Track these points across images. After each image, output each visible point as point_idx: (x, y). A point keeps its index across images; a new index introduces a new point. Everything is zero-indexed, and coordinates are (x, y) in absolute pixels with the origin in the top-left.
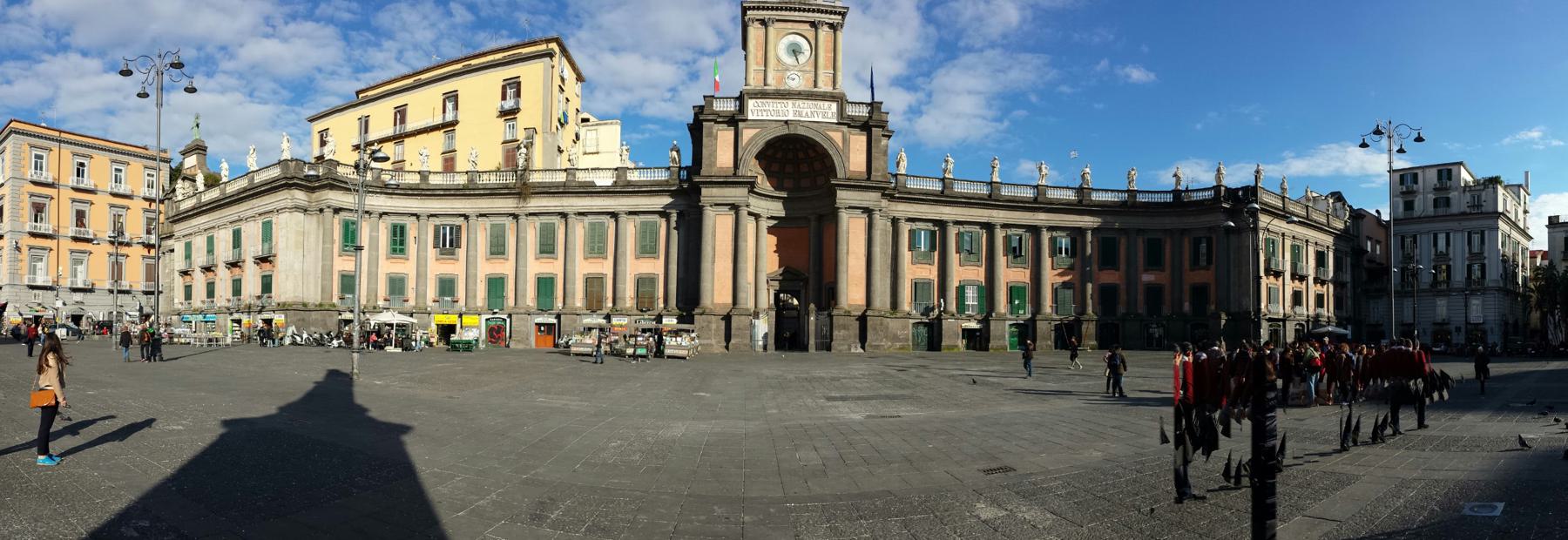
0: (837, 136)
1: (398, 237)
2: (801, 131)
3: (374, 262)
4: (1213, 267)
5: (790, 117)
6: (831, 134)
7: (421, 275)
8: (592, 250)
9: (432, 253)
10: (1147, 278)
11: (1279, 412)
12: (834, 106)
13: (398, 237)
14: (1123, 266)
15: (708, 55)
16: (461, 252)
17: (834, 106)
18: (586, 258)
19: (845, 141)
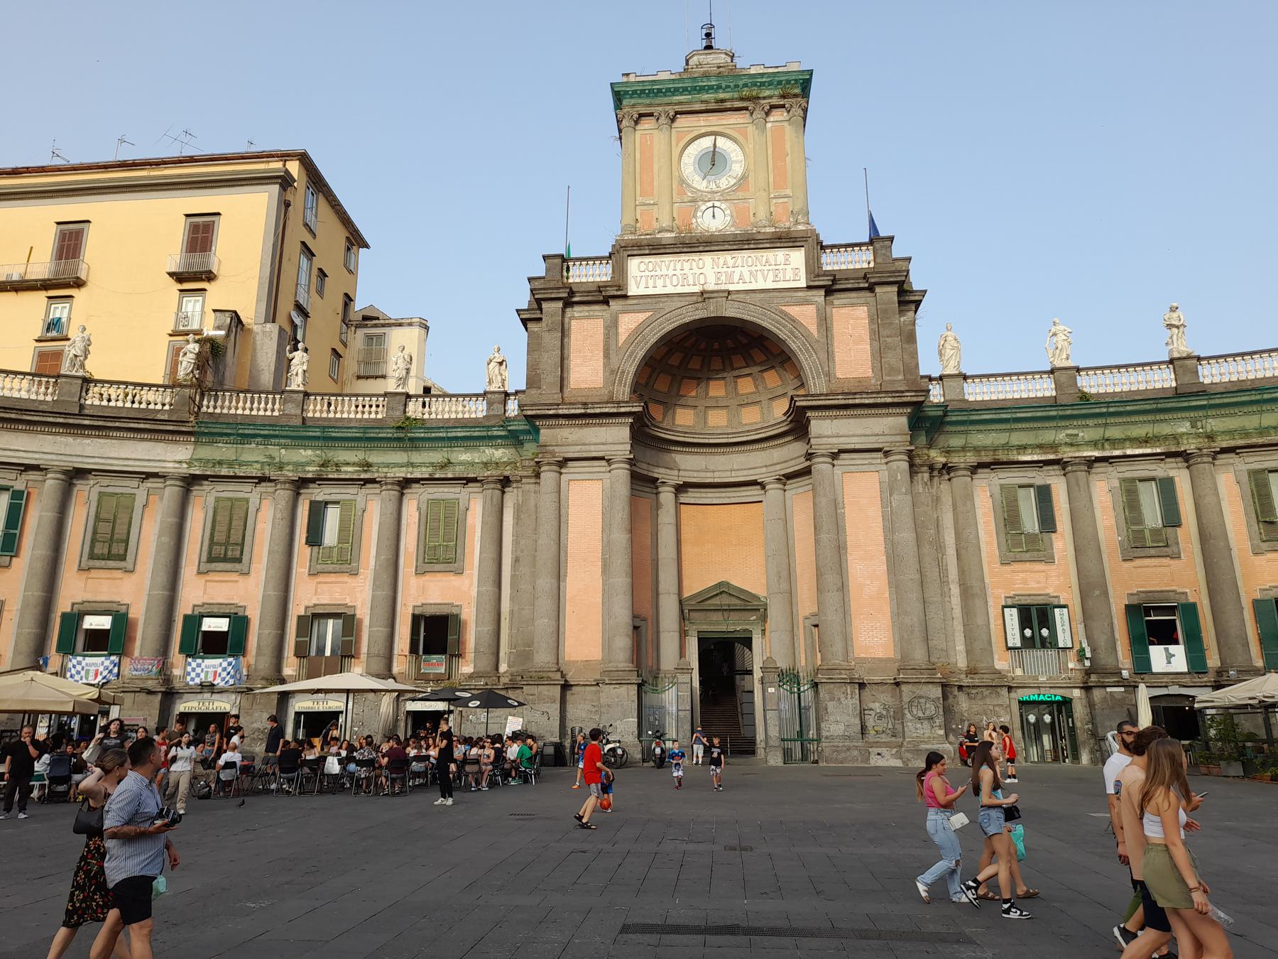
0: (806, 314)
6: (793, 311)
12: (797, 257)
16: (1062, 542)
19: (825, 322)
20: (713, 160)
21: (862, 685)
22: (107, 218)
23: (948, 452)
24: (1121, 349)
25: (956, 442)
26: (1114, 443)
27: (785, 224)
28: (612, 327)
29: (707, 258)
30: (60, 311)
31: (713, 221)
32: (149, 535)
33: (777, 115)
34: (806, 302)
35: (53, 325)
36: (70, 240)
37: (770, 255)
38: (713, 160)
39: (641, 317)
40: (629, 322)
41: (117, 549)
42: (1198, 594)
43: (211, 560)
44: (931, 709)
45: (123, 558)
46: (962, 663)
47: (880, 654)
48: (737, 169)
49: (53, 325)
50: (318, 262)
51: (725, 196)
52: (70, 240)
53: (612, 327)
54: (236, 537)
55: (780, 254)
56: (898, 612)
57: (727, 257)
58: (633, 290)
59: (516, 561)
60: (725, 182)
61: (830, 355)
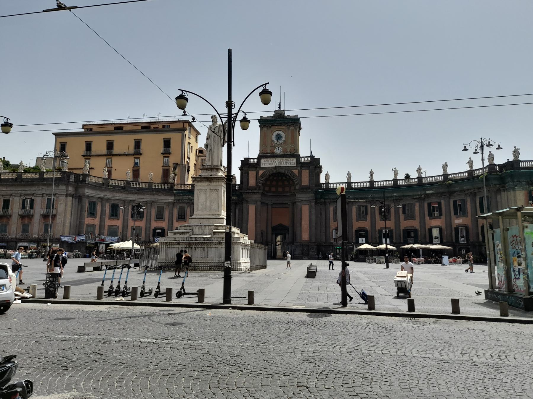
0: (296, 172)
1: (114, 213)
2: (281, 171)
3: (102, 221)
4: (443, 217)
5: (277, 165)
6: (294, 171)
7: (101, 226)
8: (112, 216)
9: (402, 216)
10: (458, 221)
11: (307, 171)
12: (295, 160)
13: (114, 213)
14: (469, 215)
15: (528, 277)
16: (369, 217)
17: (295, 160)
18: (109, 219)
19: (300, 173)
20: (279, 137)
21: (302, 245)
22: (146, 139)
23: (325, 199)
24: (442, 154)
25: (326, 197)
26: (357, 199)
27: (293, 153)
28: (257, 173)
29: (277, 159)
30: (137, 161)
31: (279, 150)
32: (166, 214)
33: (292, 127)
34: (296, 169)
35: (136, 164)
36: (138, 144)
37: (289, 159)
38: (279, 137)
39: (263, 171)
40: (261, 172)
41: (161, 217)
42: (369, 229)
43: (179, 218)
44: (314, 250)
45: (162, 218)
46: (324, 241)
47: (306, 239)
48: (284, 139)
49: (136, 164)
50: (191, 145)
51: (281, 145)
52: (138, 144)
53: (257, 173)
54: (183, 214)
55: (291, 159)
56: (310, 232)
57: (281, 159)
58: (262, 166)
59: (239, 220)
60: (281, 142)
61: (301, 180)
